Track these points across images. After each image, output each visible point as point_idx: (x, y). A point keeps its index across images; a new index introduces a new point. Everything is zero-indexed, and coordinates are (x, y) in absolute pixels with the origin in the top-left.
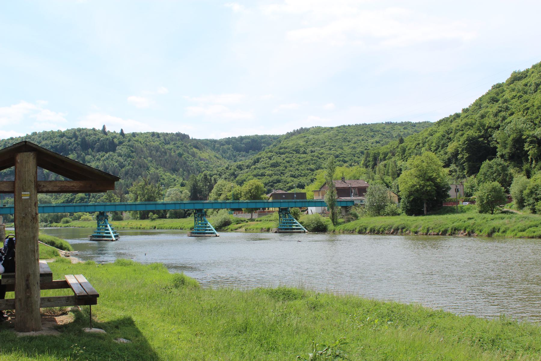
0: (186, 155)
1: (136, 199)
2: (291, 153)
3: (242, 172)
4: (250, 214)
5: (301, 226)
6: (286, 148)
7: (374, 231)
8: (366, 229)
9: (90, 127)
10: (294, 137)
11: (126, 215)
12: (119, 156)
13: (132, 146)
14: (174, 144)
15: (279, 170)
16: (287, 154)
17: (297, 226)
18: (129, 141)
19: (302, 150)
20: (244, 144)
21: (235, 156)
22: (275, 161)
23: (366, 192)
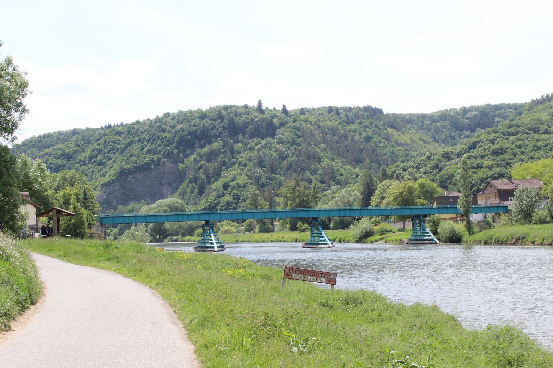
0: (376, 138)
1: (286, 205)
2: (526, 133)
3: (450, 163)
4: (401, 223)
6: (519, 126)
7: (498, 241)
8: (491, 238)
9: (240, 103)
10: (540, 107)
11: (278, 224)
12: (279, 143)
13: (298, 129)
14: (360, 123)
15: (504, 160)
17: (429, 236)
18: (294, 121)
20: (467, 118)
21: (453, 138)
22: (498, 146)
23: (513, 196)
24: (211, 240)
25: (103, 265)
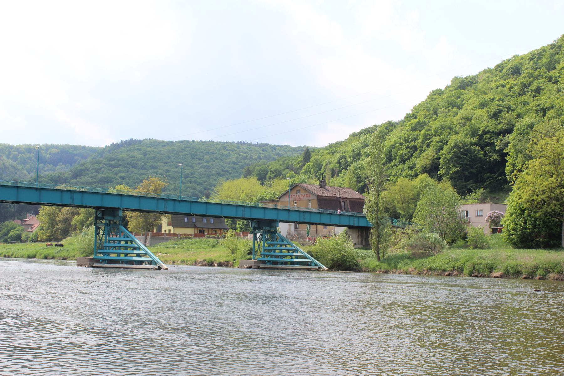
2: (125, 167)
5: (311, 259)
16: (120, 168)
19: (140, 164)
22: (105, 176)
25: (406, 268)
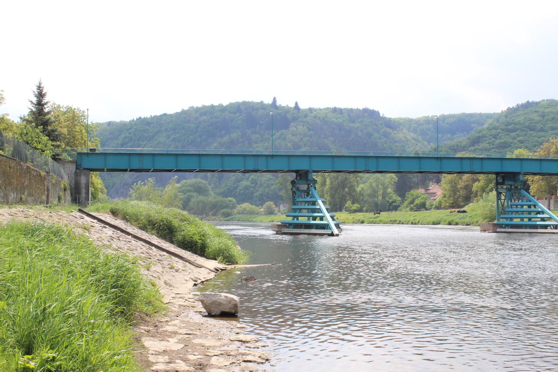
2: (523, 130)
16: (518, 132)
24: (319, 211)
